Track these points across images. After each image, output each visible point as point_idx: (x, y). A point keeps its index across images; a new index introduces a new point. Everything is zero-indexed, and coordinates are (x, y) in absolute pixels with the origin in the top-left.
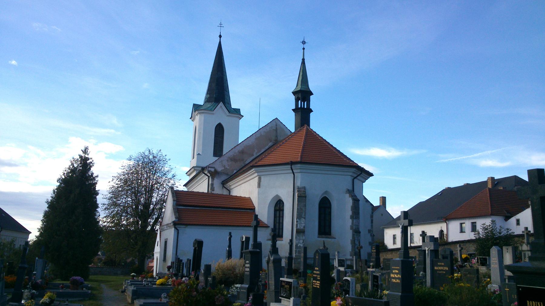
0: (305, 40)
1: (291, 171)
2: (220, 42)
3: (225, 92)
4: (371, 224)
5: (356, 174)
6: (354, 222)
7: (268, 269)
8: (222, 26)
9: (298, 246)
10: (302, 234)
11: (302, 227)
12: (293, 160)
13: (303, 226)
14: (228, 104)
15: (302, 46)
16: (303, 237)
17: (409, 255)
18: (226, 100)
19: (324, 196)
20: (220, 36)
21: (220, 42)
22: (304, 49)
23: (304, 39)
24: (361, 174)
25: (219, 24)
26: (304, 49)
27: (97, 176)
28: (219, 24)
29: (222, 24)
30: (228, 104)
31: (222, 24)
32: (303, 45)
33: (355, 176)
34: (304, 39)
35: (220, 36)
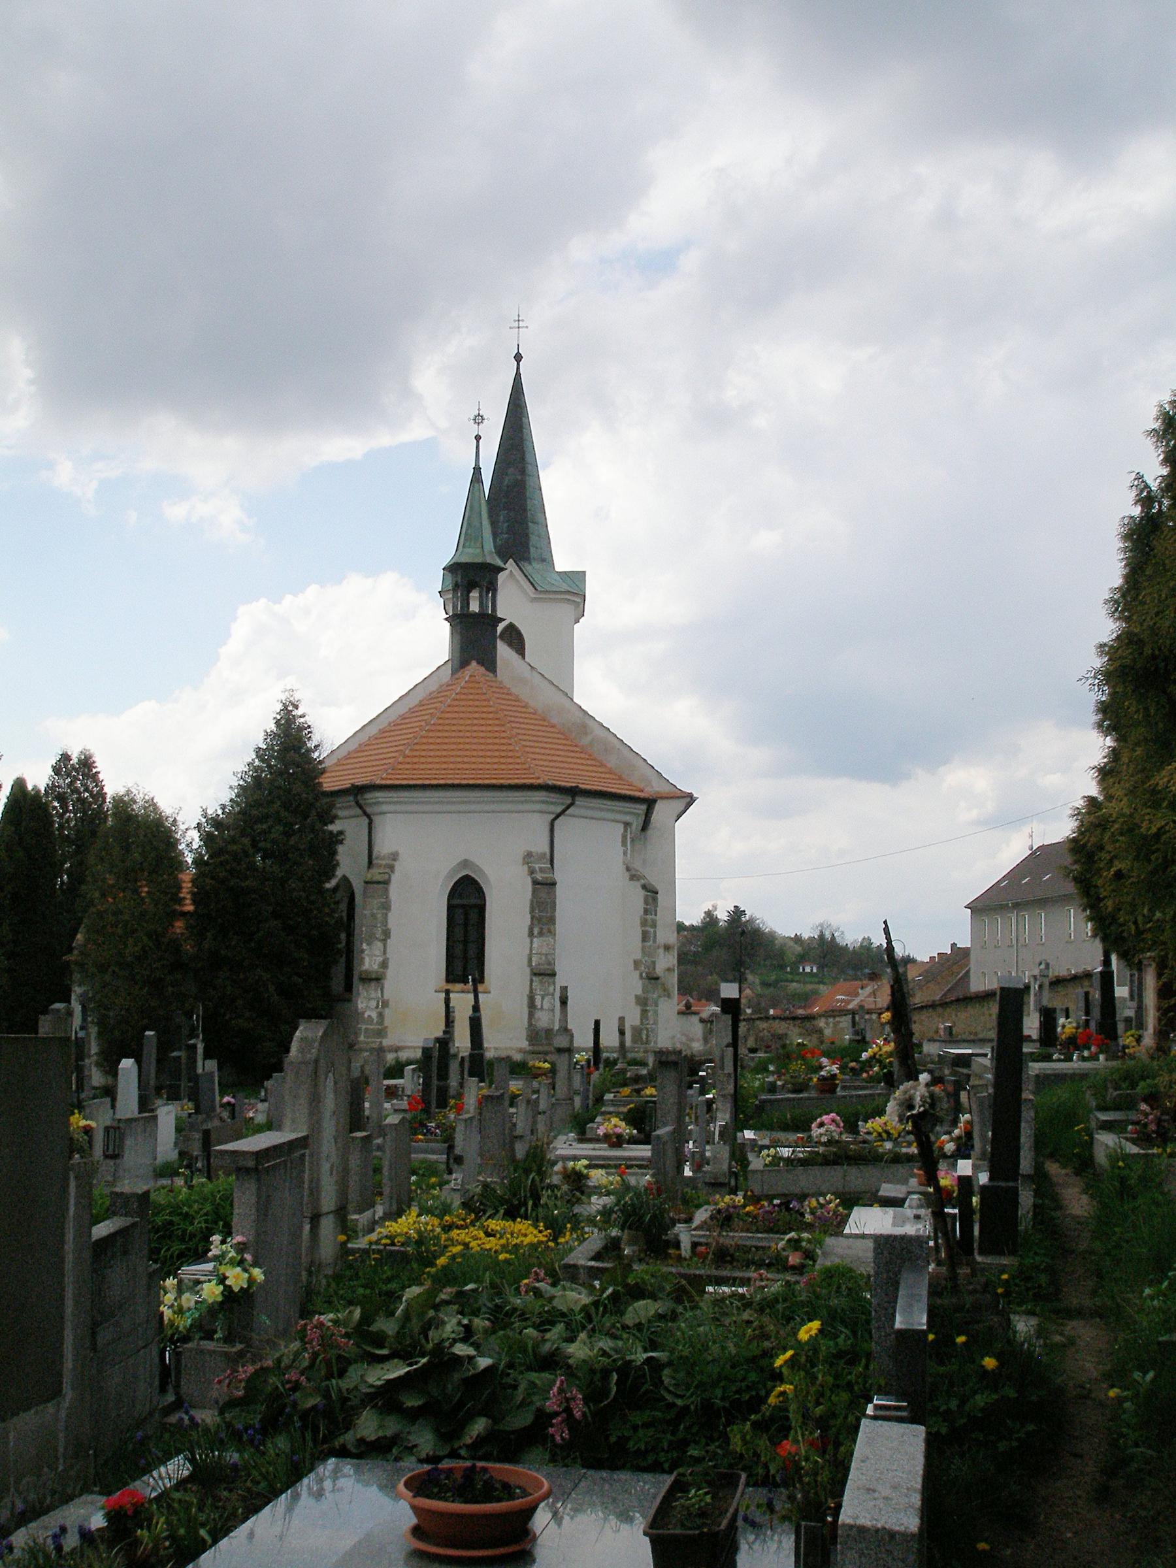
0: (481, 413)
1: (359, 811)
2: (518, 376)
3: (530, 524)
4: (640, 945)
5: (562, 804)
6: (535, 945)
7: (463, 1078)
8: (521, 324)
9: (366, 1016)
10: (373, 984)
11: (376, 967)
12: (360, 782)
13: (377, 962)
14: (543, 560)
15: (474, 430)
16: (376, 990)
17: (1022, 1032)
18: (532, 550)
19: (460, 876)
20: (518, 358)
21: (518, 376)
22: (478, 438)
23: (479, 410)
24: (573, 800)
25: (515, 321)
26: (478, 438)
27: (205, 811)
28: (515, 321)
29: (523, 320)
30: (543, 560)
31: (523, 320)
32: (476, 426)
33: (559, 809)
34: (479, 410)
35: (518, 358)
